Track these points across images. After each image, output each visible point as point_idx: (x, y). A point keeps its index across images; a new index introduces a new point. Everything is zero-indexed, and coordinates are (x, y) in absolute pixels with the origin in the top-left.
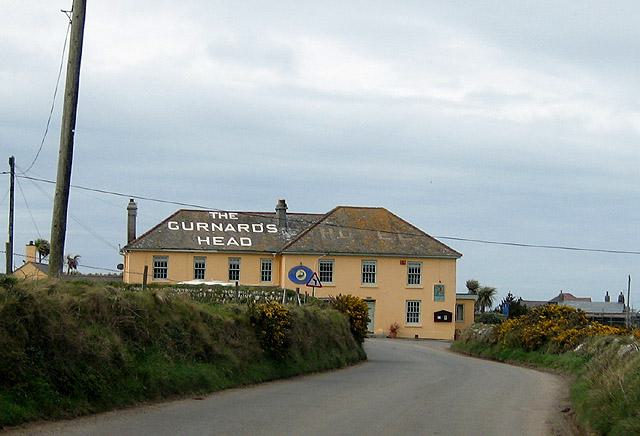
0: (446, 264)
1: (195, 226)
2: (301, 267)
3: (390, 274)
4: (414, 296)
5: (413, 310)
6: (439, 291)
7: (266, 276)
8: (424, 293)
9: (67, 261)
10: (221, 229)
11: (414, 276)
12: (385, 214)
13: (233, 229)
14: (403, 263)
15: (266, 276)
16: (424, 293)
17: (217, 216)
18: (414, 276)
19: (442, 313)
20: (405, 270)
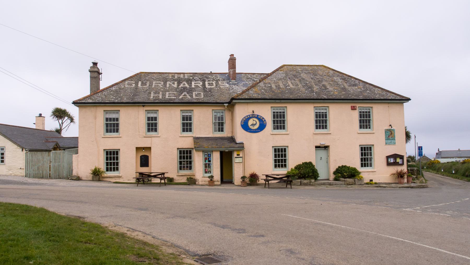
0: (394, 108)
1: (151, 84)
2: (254, 116)
3: (343, 118)
4: (366, 140)
5: (366, 154)
6: (390, 135)
7: (220, 126)
8: (375, 137)
9: (26, 179)
10: (175, 85)
11: (365, 121)
12: (361, 85)
13: (187, 85)
14: (353, 108)
15: (220, 126)
16: (375, 137)
17: (173, 76)
18: (365, 121)
19: (395, 156)
20: (356, 114)
